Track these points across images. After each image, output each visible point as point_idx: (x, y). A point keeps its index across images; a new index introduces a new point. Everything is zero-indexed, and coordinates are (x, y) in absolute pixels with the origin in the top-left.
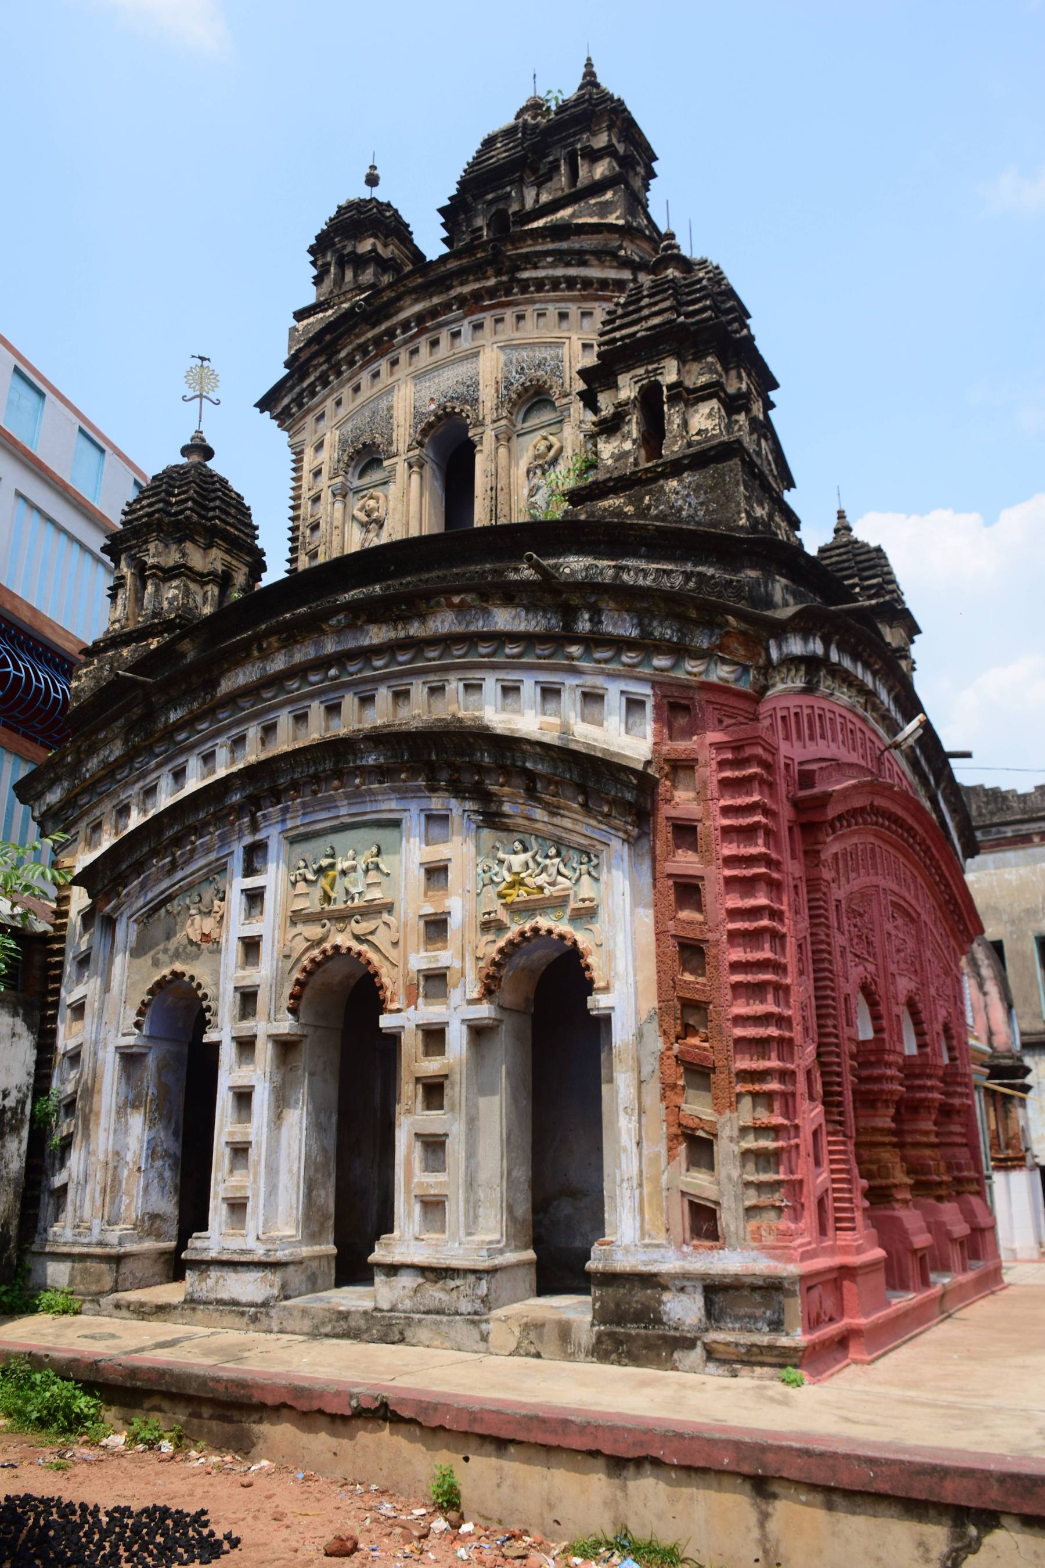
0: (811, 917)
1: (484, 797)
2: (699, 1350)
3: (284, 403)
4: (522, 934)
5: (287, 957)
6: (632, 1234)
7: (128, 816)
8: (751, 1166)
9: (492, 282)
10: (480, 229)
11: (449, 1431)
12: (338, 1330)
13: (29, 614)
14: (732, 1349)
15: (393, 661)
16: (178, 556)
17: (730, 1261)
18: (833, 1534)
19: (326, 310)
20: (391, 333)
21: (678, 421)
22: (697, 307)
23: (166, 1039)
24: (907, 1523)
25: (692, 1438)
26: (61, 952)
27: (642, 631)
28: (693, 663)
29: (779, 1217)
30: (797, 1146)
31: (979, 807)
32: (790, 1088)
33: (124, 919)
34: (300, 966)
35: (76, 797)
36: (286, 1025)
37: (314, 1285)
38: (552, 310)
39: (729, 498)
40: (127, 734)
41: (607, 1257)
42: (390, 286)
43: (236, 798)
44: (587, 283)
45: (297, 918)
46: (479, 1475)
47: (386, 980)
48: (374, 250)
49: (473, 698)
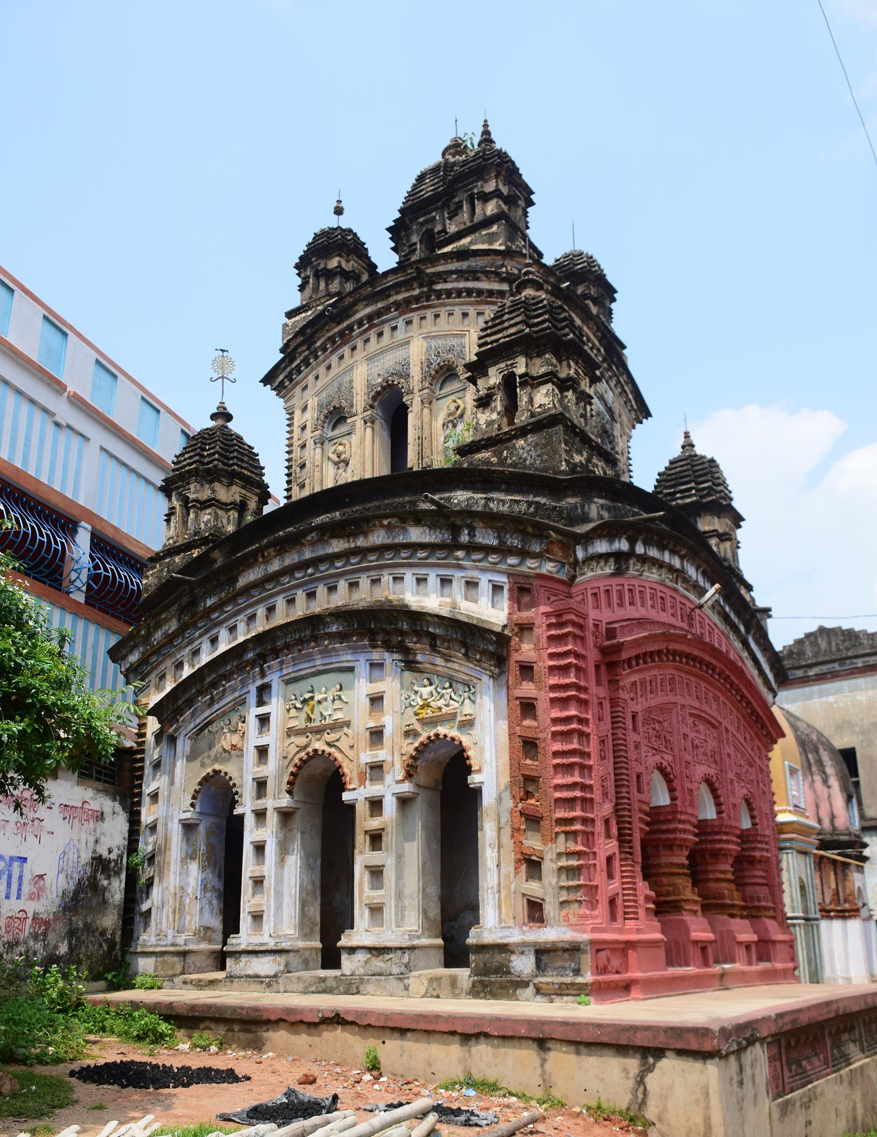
1: (406, 651)
2: (531, 989)
3: (281, 379)
4: (429, 738)
5: (285, 758)
6: (495, 920)
7: (182, 669)
8: (564, 877)
9: (417, 292)
10: (415, 244)
11: (374, 1027)
12: (320, 989)
13: (112, 531)
14: (550, 987)
15: (348, 562)
16: (210, 492)
18: (579, 1067)
19: (307, 311)
20: (350, 328)
21: (525, 399)
22: (539, 319)
23: (211, 815)
24: (618, 1059)
25: (505, 1020)
26: (142, 760)
27: (500, 541)
28: (532, 561)
29: (580, 907)
30: (595, 865)
31: (837, 644)
32: (590, 829)
34: (293, 763)
35: (148, 657)
36: (285, 801)
37: (306, 965)
38: (458, 311)
40: (180, 614)
41: (479, 935)
42: (350, 294)
43: (250, 655)
44: (480, 292)
45: (291, 732)
46: (391, 1050)
47: (346, 770)
48: (339, 266)
49: (399, 586)
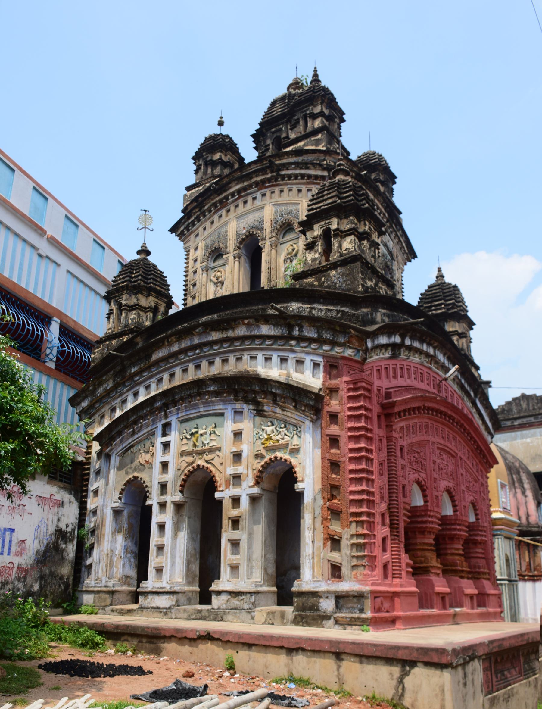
0: (388, 452)
1: (257, 404)
2: (332, 621)
4: (271, 459)
7: (115, 412)
8: (354, 550)
9: (269, 176)
10: (269, 145)
12: (198, 617)
14: (344, 620)
16: (135, 300)
17: (345, 586)
18: (362, 672)
19: (199, 187)
20: (226, 198)
21: (337, 245)
22: (347, 194)
23: (132, 505)
26: (89, 469)
27: (319, 335)
30: (375, 543)
31: (533, 405)
32: (372, 520)
33: (114, 455)
34: (184, 473)
36: (178, 497)
37: (190, 602)
38: (295, 188)
39: (355, 279)
40: (115, 377)
41: (300, 586)
42: (227, 176)
43: (158, 404)
45: (183, 453)
46: (242, 658)
47: (217, 479)
48: (220, 158)
49: (253, 362)
